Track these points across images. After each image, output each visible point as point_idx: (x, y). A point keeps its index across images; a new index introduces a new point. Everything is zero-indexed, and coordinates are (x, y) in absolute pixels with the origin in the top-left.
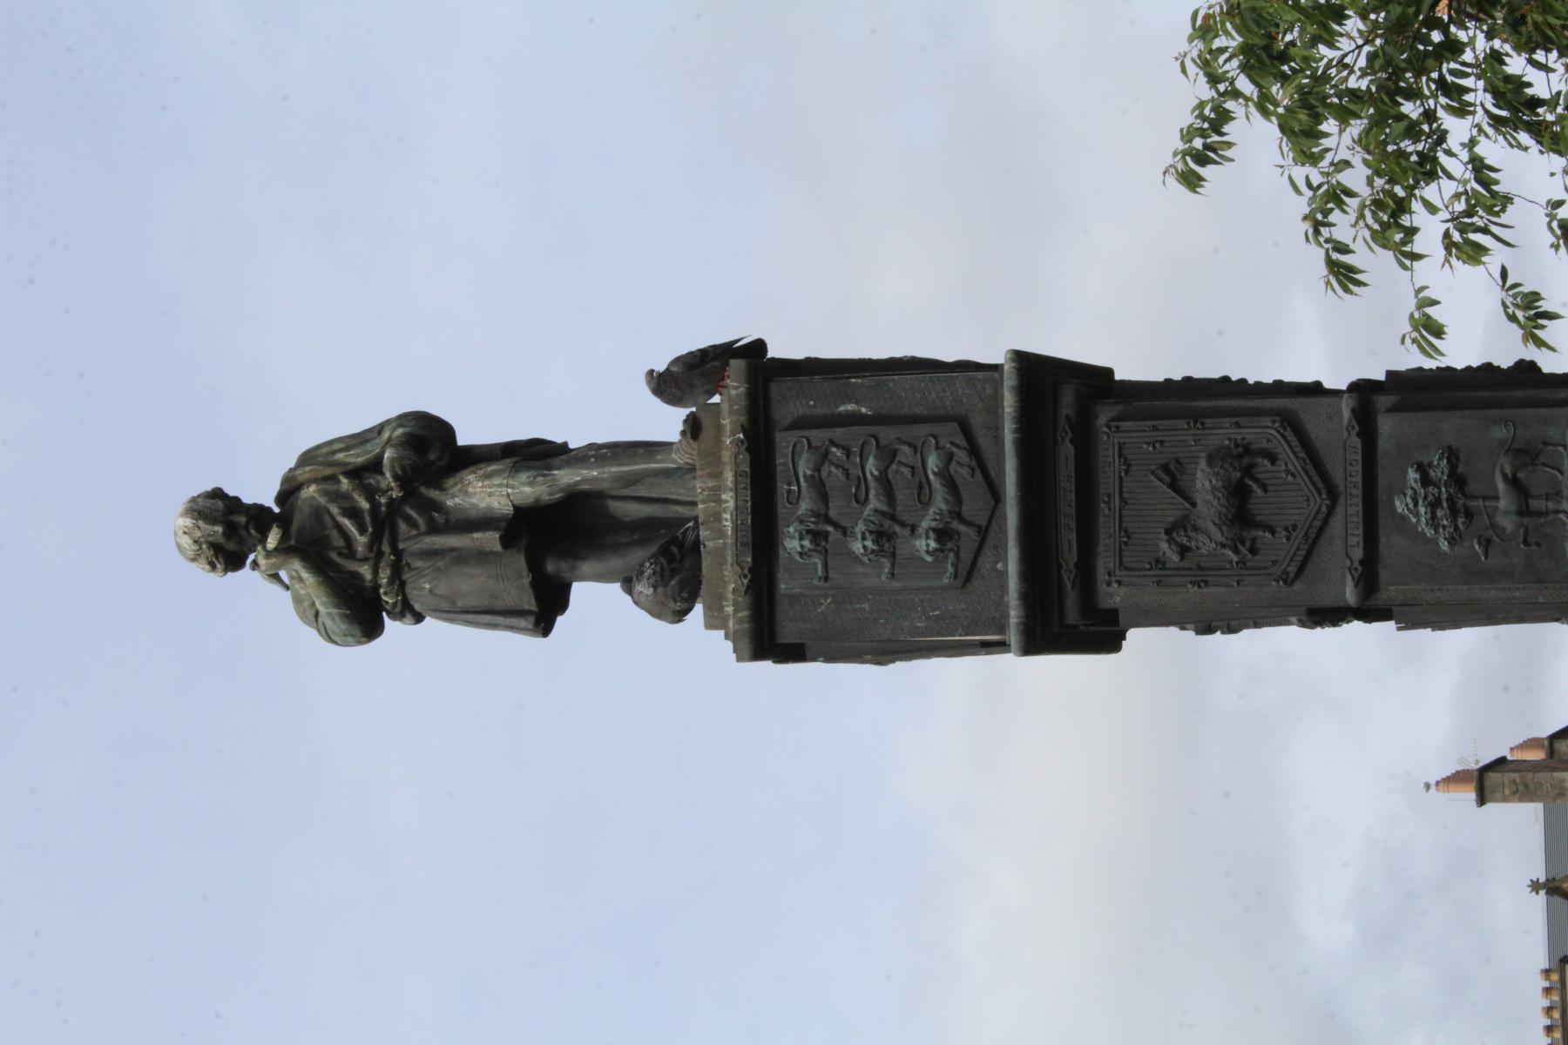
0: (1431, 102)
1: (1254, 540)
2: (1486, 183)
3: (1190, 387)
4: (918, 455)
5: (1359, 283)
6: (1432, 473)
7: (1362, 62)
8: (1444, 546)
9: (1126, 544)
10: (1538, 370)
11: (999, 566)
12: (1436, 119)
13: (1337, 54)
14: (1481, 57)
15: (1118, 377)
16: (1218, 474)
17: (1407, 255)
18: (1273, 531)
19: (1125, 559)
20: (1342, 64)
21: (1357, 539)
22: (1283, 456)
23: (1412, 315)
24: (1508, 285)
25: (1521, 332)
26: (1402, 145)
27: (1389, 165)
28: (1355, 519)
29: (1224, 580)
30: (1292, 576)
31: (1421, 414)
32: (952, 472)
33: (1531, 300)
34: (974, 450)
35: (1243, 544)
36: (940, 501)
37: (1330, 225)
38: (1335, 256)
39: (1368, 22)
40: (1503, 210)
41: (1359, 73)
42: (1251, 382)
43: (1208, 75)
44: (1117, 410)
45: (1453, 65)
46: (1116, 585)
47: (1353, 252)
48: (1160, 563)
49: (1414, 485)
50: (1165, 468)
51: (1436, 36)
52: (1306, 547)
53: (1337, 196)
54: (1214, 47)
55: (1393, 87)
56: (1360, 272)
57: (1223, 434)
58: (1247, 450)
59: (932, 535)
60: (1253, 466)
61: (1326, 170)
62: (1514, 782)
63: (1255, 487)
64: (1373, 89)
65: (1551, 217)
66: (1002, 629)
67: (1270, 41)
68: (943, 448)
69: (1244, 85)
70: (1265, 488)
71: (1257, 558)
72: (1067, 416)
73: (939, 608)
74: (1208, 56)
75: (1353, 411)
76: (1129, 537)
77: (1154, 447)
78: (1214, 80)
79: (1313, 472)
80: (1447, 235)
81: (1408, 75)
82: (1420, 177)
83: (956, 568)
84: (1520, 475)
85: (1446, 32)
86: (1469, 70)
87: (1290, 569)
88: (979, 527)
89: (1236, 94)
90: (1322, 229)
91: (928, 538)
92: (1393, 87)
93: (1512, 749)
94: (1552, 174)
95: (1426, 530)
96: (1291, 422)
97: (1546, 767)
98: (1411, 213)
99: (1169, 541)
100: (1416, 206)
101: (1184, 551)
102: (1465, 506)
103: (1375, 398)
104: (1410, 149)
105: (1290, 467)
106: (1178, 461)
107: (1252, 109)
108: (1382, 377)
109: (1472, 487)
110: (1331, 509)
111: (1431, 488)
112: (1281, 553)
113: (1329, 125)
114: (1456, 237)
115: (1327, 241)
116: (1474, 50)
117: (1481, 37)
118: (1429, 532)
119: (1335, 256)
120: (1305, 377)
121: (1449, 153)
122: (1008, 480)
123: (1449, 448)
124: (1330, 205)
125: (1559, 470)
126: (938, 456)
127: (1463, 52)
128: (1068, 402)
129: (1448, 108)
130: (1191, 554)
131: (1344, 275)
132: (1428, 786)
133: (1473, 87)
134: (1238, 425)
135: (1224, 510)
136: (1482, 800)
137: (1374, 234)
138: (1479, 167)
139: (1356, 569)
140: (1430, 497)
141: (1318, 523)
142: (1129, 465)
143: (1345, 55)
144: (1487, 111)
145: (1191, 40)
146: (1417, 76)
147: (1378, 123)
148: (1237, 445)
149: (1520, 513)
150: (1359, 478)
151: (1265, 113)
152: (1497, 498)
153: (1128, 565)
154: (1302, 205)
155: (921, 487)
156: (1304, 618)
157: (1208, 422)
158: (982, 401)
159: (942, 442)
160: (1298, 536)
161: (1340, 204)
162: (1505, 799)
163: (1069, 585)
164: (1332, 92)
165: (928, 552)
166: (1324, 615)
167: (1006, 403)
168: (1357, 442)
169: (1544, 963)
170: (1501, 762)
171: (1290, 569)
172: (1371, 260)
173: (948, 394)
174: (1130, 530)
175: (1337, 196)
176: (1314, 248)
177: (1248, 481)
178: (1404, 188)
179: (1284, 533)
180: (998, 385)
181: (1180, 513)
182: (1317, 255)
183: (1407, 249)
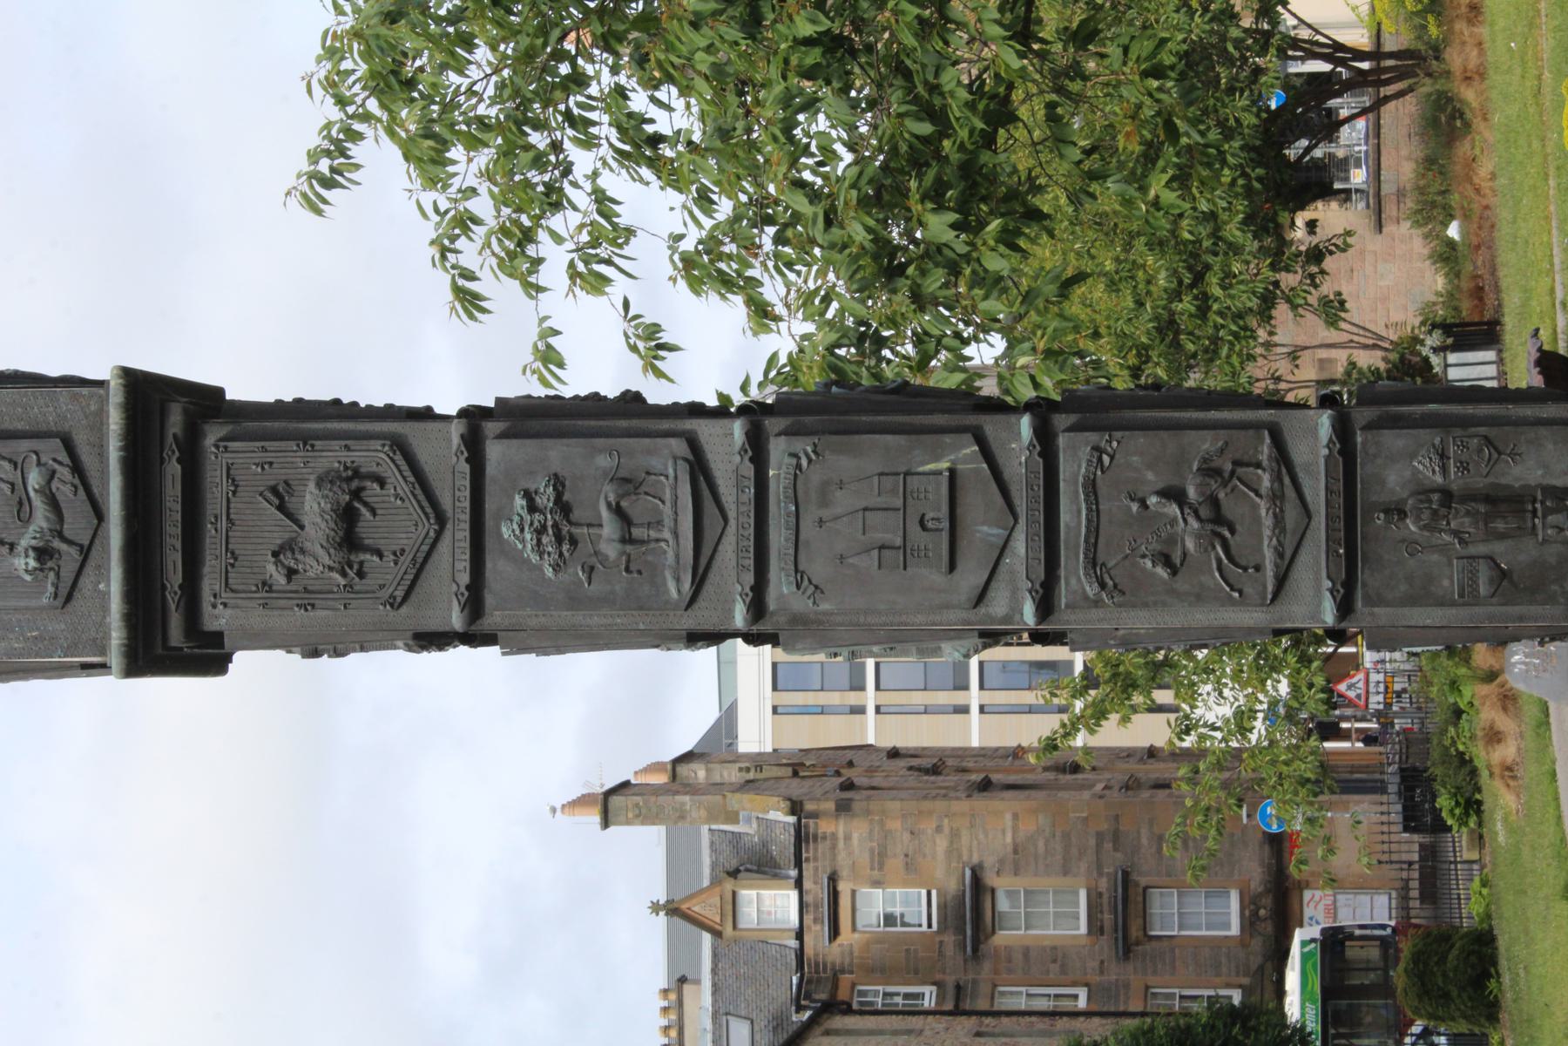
0: (558, 134)
1: (361, 563)
2: (607, 215)
3: (301, 409)
4: (19, 471)
5: (484, 311)
6: (538, 500)
7: (491, 91)
8: (549, 572)
9: (233, 565)
10: (643, 401)
11: (101, 586)
12: (562, 151)
13: (466, 82)
14: (607, 90)
15: (228, 397)
16: (327, 497)
17: (531, 285)
18: (381, 556)
19: (230, 581)
20: (470, 92)
21: (464, 564)
22: (392, 480)
23: (535, 345)
24: (630, 316)
25: (641, 363)
26: (529, 175)
27: (513, 194)
28: (462, 544)
29: (330, 603)
30: (399, 600)
31: (528, 442)
32: (54, 490)
33: (653, 330)
34: (77, 468)
35: (351, 567)
36: (41, 516)
37: (456, 252)
38: (461, 282)
39: (498, 54)
40: (627, 242)
41: (488, 102)
42: (363, 405)
43: (334, 96)
44: (223, 431)
45: (580, 98)
46: (221, 607)
47: (478, 279)
48: (266, 585)
49: (520, 512)
50: (274, 490)
51: (564, 69)
52: (414, 571)
53: (465, 222)
54: (342, 68)
55: (520, 117)
56: (485, 299)
57: (332, 457)
58: (356, 474)
59: (31, 553)
60: (362, 489)
61: (454, 196)
62: (637, 805)
63: (363, 510)
64: (502, 117)
65: (673, 249)
66: (103, 651)
67: (1427, 87)
68: (45, 465)
69: (373, 105)
70: (373, 512)
71: (364, 581)
72: (175, 436)
73: (38, 629)
74: (336, 78)
75: (462, 436)
76: (236, 559)
77: (263, 468)
78: (341, 102)
79: (422, 497)
80: (572, 265)
81: (536, 106)
82: (546, 207)
83: (57, 588)
84: (624, 504)
85: (574, 65)
86: (594, 104)
87: (397, 593)
88: (81, 546)
89: (366, 117)
90: (449, 255)
91: (27, 556)
92: (520, 117)
93: (636, 773)
94: (672, 209)
95: (532, 556)
96: (401, 447)
97: (669, 791)
98: (537, 243)
99: (276, 564)
100: (542, 235)
101: (291, 573)
102: (569, 532)
103: (484, 424)
104: (535, 180)
105: (399, 491)
106: (286, 482)
107: (381, 133)
108: (491, 404)
109: (576, 515)
110: (439, 534)
111: (537, 515)
112: (388, 577)
113: (457, 153)
114: (581, 267)
115: (453, 267)
116: (599, 83)
117: (606, 71)
118: (535, 558)
119: (461, 282)
120: (417, 401)
121: (575, 185)
122: (111, 499)
123: (556, 475)
124: (457, 231)
125: (660, 500)
126: (40, 472)
127: (589, 85)
128: (175, 421)
129: (575, 140)
130: (298, 576)
131: (469, 301)
132: (554, 810)
133: (598, 120)
134: (347, 448)
135: (332, 533)
136: (606, 823)
137: (501, 260)
138: (602, 200)
139: (462, 594)
140: (536, 524)
141: (425, 548)
142: (237, 486)
143: (475, 83)
144: (611, 145)
145: (319, 60)
146: (545, 107)
147: (506, 153)
148: (346, 468)
149: (623, 541)
150: (467, 504)
151: (391, 133)
152: (601, 525)
153: (234, 587)
154: (429, 230)
155: (20, 503)
156: (411, 642)
157: (318, 444)
158: (87, 417)
159: (43, 460)
160: (406, 561)
161: (466, 230)
162: (628, 823)
163: (173, 607)
164: (461, 119)
165: (26, 571)
166: (430, 640)
167: (111, 420)
168: (466, 468)
169: (663, 983)
170: (625, 785)
171: (397, 593)
172: (497, 289)
173: (51, 409)
174: (237, 552)
175: (465, 222)
176: (440, 272)
177: (357, 505)
178: (530, 218)
179: (392, 557)
180: (104, 400)
181: (287, 536)
182: (443, 280)
183: (532, 279)
